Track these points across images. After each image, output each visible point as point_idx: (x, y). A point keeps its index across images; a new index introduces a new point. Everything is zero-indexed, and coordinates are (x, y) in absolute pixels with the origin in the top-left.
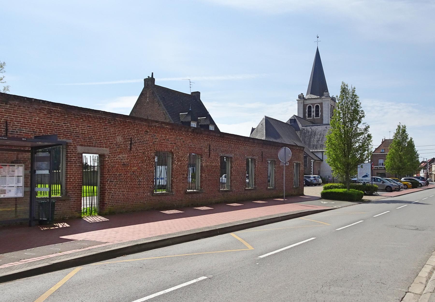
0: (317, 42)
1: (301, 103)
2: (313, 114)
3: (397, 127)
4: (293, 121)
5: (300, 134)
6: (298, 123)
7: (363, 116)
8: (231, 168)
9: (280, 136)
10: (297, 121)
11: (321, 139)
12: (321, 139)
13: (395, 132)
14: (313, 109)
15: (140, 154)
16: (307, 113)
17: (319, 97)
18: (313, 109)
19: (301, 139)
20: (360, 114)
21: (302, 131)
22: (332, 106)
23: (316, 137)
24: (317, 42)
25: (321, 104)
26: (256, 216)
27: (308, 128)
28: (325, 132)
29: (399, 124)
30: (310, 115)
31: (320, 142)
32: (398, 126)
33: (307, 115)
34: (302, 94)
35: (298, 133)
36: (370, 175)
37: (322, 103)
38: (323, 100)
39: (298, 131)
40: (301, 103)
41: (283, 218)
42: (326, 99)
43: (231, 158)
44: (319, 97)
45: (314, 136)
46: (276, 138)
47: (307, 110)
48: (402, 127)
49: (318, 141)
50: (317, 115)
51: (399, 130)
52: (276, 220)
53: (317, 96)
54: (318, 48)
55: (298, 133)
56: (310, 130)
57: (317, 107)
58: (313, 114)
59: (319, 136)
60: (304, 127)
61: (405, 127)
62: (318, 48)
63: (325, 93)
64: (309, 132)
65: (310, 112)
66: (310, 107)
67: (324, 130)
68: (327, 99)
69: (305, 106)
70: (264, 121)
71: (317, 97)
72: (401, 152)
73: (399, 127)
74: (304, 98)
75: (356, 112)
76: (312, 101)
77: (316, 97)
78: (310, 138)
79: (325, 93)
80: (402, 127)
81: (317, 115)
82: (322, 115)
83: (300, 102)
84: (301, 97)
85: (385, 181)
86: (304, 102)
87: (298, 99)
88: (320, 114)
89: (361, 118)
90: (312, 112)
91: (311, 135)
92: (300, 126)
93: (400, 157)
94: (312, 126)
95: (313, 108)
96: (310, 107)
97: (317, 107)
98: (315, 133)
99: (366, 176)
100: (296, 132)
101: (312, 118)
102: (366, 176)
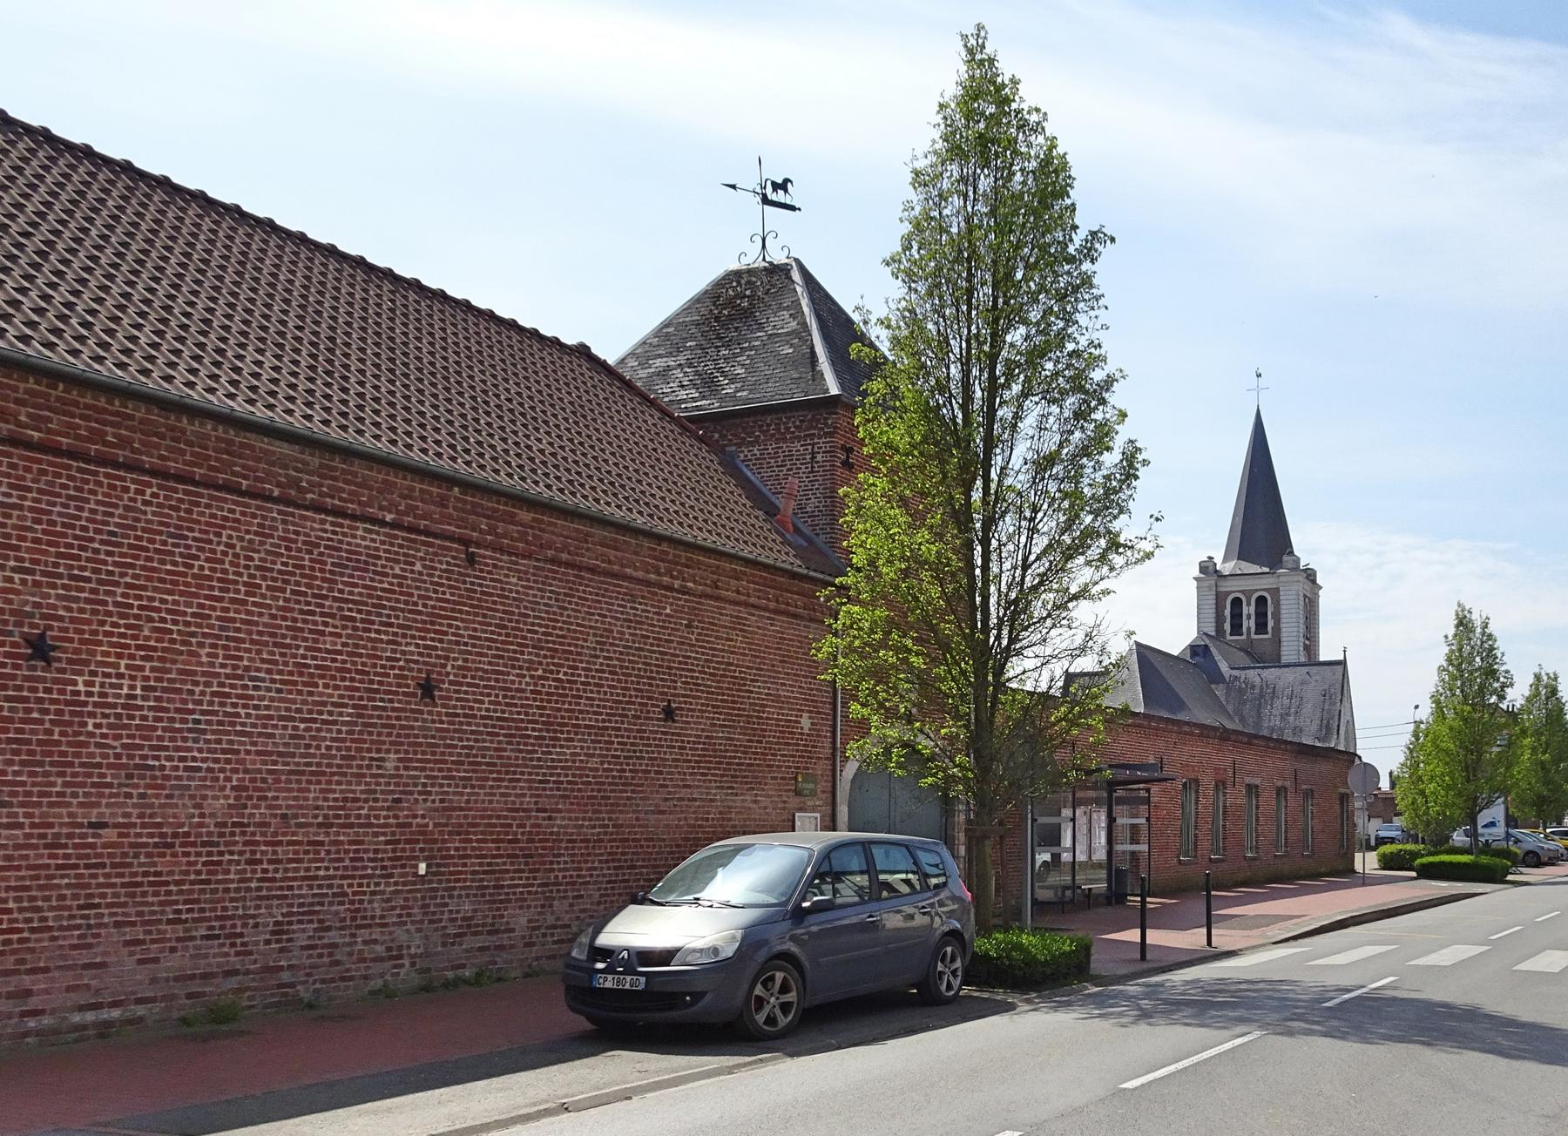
0: (1258, 389)
1: (1210, 588)
2: (1249, 624)
3: (1531, 680)
4: (1194, 649)
5: (1228, 694)
6: (1218, 657)
7: (1512, 685)
8: (1257, 808)
9: (1184, 703)
10: (1213, 650)
11: (1293, 710)
12: (1293, 710)
13: (1527, 693)
14: (1249, 610)
15: (160, 719)
16: (1228, 620)
17: (1266, 570)
18: (1249, 610)
19: (1230, 708)
20: (1502, 679)
21: (1229, 685)
22: (1305, 596)
23: (1277, 703)
24: (1258, 389)
25: (1275, 592)
26: (1364, 905)
27: (1251, 673)
28: (1304, 687)
29: (1537, 670)
30: (1237, 628)
31: (1291, 719)
32: (1535, 675)
33: (1227, 626)
34: (1211, 558)
35: (1220, 691)
36: (1502, 823)
37: (1277, 590)
38: (1281, 579)
39: (1217, 683)
40: (1210, 588)
41: (1374, 916)
42: (1290, 578)
43: (1257, 786)
44: (1266, 570)
45: (1272, 699)
46: (1172, 710)
47: (1227, 612)
48: (1545, 678)
49: (1283, 717)
50: (1261, 627)
51: (1537, 689)
52: (1363, 919)
53: (1261, 565)
54: (1258, 411)
55: (1220, 691)
56: (1257, 680)
57: (1261, 601)
58: (1249, 624)
59: (1286, 702)
60: (1236, 673)
61: (1556, 679)
62: (1258, 411)
63: (1285, 558)
64: (1253, 687)
65: (1237, 616)
66: (1237, 603)
67: (1303, 683)
68: (1296, 578)
69: (1220, 598)
70: (1135, 656)
71: (1260, 571)
72: (1545, 752)
73: (1538, 677)
74: (1216, 571)
75: (1491, 673)
76: (1243, 582)
77: (1256, 569)
78: (1260, 705)
79: (1285, 558)
80: (1545, 678)
81: (1261, 627)
82: (1277, 629)
83: (1206, 584)
84: (1207, 568)
85: (1520, 836)
86: (1220, 584)
87: (1196, 573)
88: (1271, 624)
89: (1503, 686)
90: (1244, 617)
91: (1262, 695)
92: (1224, 667)
93: (1543, 769)
94: (1263, 668)
95: (1249, 604)
96: (1237, 603)
97: (1261, 601)
98: (1274, 692)
99: (1492, 824)
100: (1213, 686)
101: (1244, 637)
102: (1492, 824)
